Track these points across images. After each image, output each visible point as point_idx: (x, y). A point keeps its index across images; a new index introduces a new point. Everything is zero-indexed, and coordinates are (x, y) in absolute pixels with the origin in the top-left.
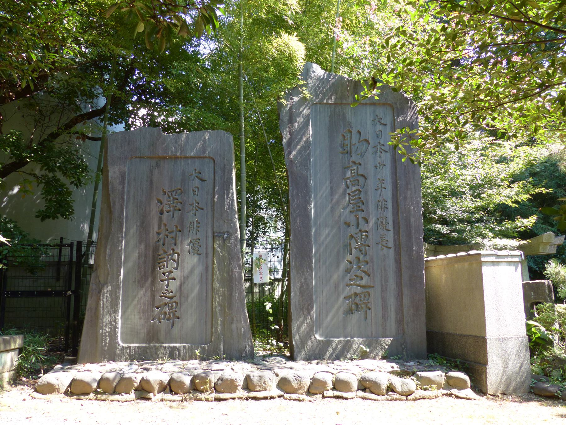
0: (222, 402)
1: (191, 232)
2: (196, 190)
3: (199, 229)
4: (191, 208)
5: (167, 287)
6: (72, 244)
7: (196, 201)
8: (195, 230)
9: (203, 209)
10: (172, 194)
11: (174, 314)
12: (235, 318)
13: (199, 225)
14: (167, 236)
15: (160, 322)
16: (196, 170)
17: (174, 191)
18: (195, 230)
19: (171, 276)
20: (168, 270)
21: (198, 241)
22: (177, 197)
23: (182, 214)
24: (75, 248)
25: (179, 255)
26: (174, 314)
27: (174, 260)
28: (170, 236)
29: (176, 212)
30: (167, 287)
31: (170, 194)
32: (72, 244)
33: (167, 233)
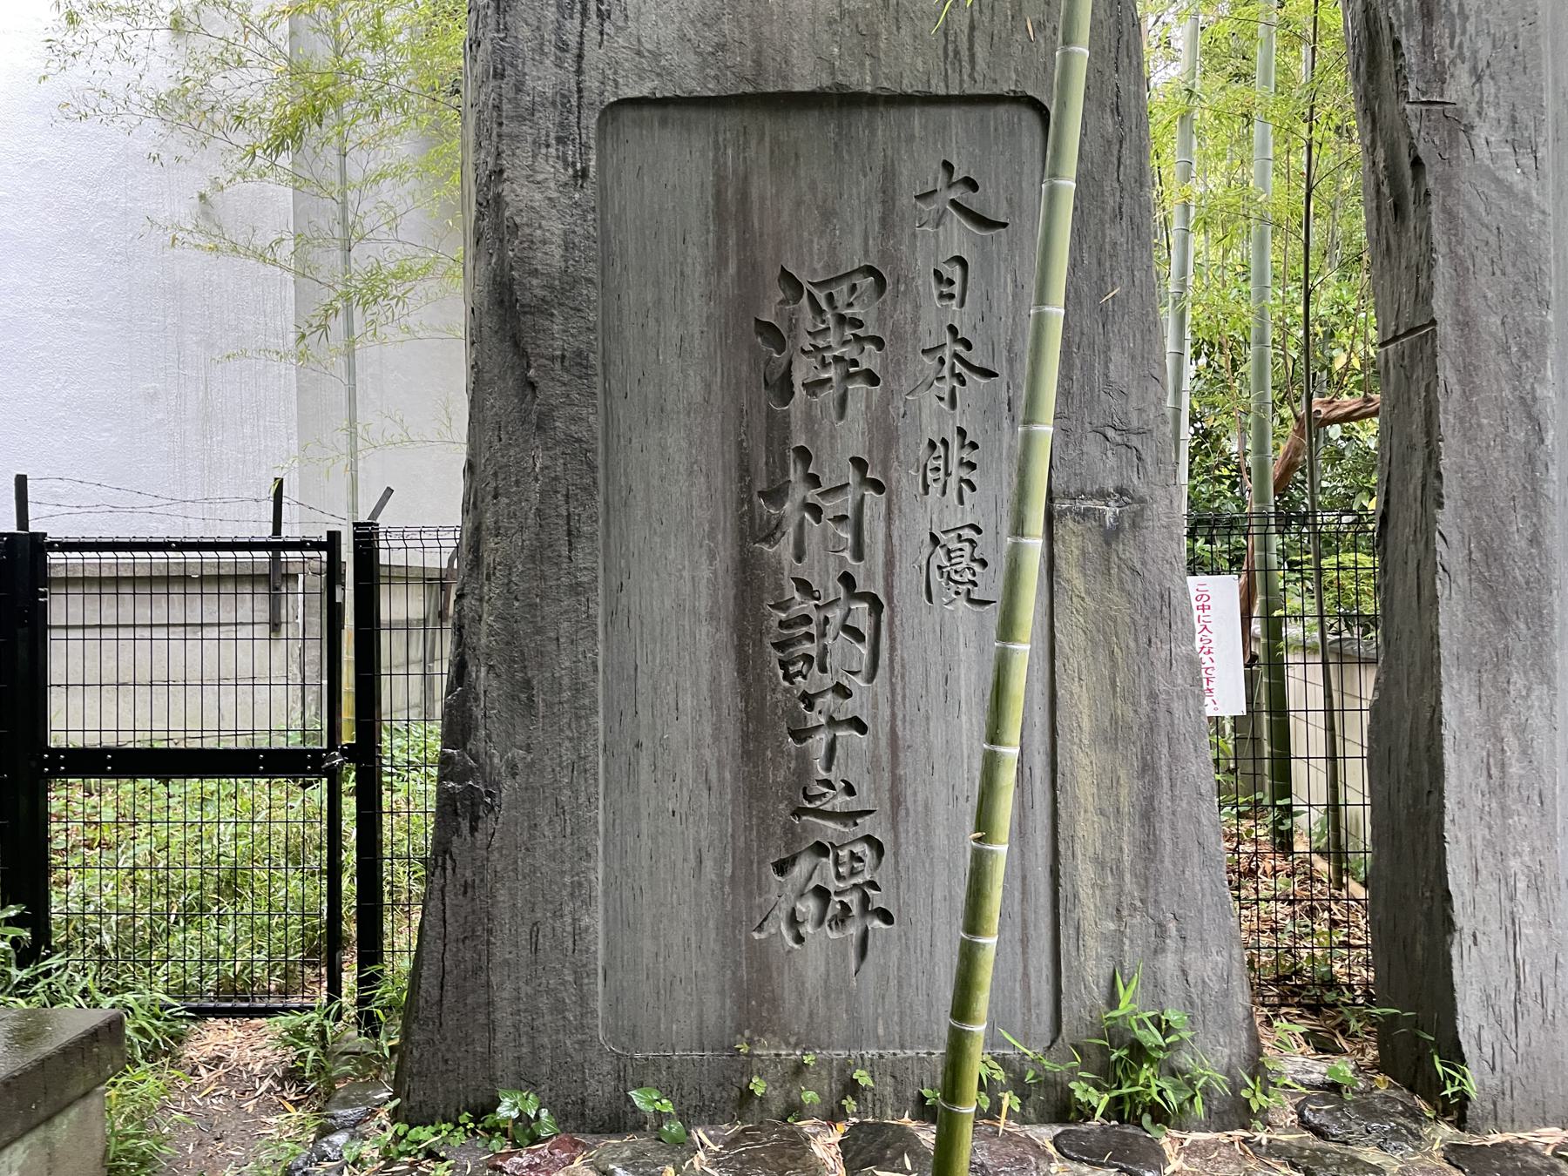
0: (861, 119)
1: (935, 488)
2: (955, 273)
3: (974, 477)
4: (930, 362)
5: (828, 769)
6: (334, 537)
7: (962, 432)
8: (953, 483)
9: (988, 374)
10: (830, 297)
11: (865, 900)
12: (1172, 926)
13: (972, 456)
14: (816, 511)
15: (799, 939)
16: (948, 166)
17: (838, 279)
18: (953, 483)
19: (849, 708)
20: (828, 681)
21: (968, 533)
22: (856, 311)
23: (886, 402)
24: (347, 555)
25: (874, 601)
26: (865, 900)
27: (857, 635)
28: (830, 506)
29: (858, 387)
30: (828, 769)
31: (821, 296)
32: (334, 537)
33: (812, 496)
